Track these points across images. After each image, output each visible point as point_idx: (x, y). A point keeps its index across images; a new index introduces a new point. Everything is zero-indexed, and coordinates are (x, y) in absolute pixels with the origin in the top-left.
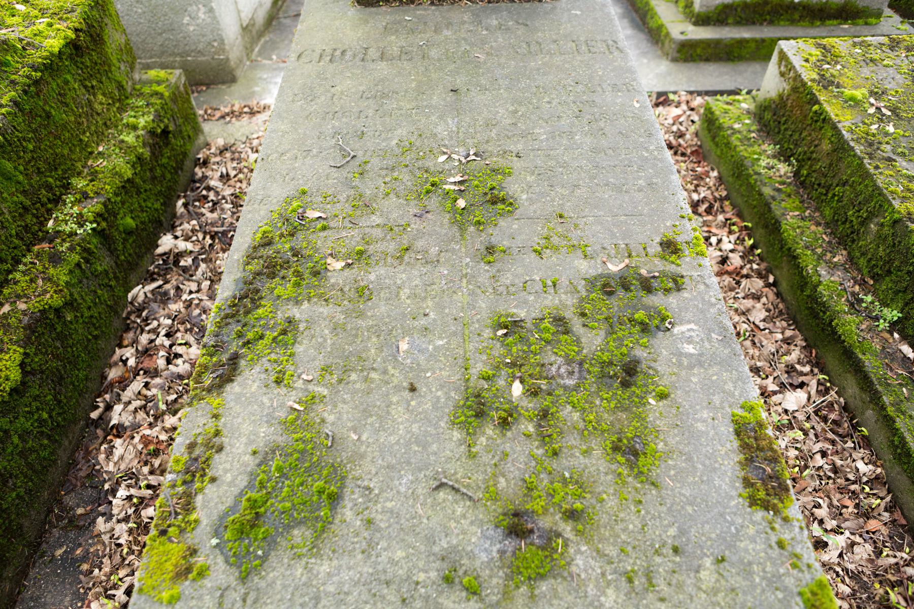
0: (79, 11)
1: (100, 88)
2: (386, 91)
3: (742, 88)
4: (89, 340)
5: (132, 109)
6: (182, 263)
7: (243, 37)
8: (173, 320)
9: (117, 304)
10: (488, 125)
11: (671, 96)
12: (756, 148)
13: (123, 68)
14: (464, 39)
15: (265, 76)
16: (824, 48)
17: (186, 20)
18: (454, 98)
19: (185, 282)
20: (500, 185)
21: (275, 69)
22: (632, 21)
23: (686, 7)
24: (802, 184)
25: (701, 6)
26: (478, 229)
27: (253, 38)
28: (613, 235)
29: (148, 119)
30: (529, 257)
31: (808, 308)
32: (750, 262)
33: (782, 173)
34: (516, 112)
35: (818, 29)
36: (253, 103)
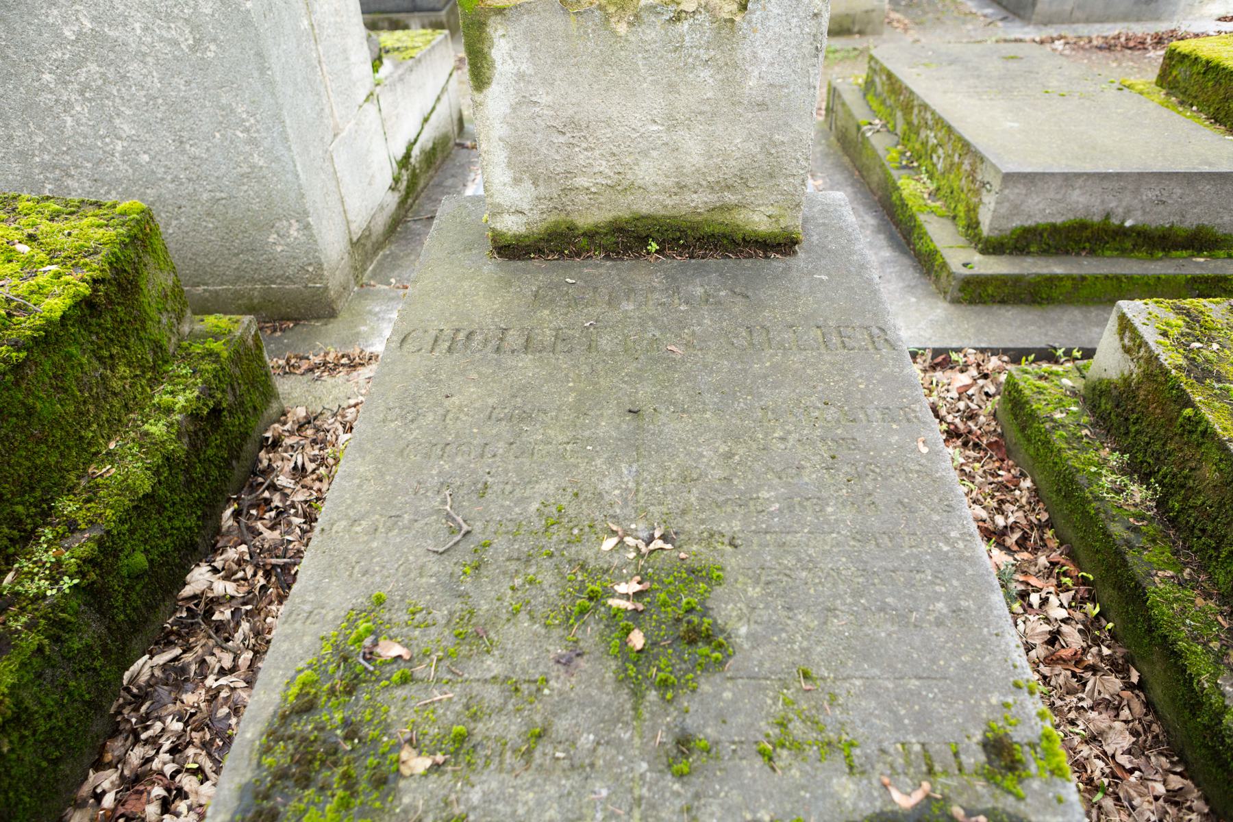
0: (104, 252)
1: (124, 356)
2: (528, 408)
3: (1057, 345)
4: (41, 771)
5: (171, 381)
6: (217, 617)
7: (351, 255)
8: (186, 724)
9: (108, 687)
10: (685, 479)
11: (954, 356)
12: (1091, 454)
13: (164, 320)
14: (653, 319)
15: (377, 309)
16: (1188, 314)
17: (273, 238)
18: (634, 424)
19: (216, 651)
20: (702, 603)
21: (392, 299)
22: (891, 238)
23: (969, 226)
24: (1172, 520)
25: (991, 230)
26: (663, 698)
27: (366, 253)
28: (897, 720)
29: (190, 396)
30: (752, 768)
31: (1206, 746)
32: (1097, 642)
33: (1138, 501)
34: (729, 455)
35: (1160, 263)
36: (354, 351)
